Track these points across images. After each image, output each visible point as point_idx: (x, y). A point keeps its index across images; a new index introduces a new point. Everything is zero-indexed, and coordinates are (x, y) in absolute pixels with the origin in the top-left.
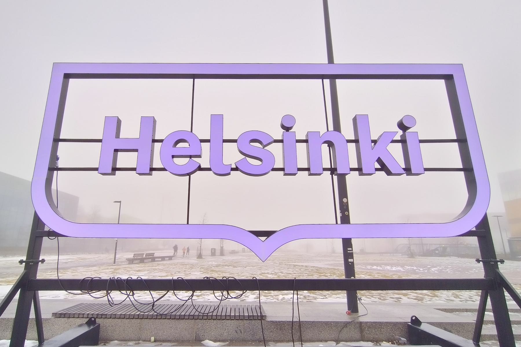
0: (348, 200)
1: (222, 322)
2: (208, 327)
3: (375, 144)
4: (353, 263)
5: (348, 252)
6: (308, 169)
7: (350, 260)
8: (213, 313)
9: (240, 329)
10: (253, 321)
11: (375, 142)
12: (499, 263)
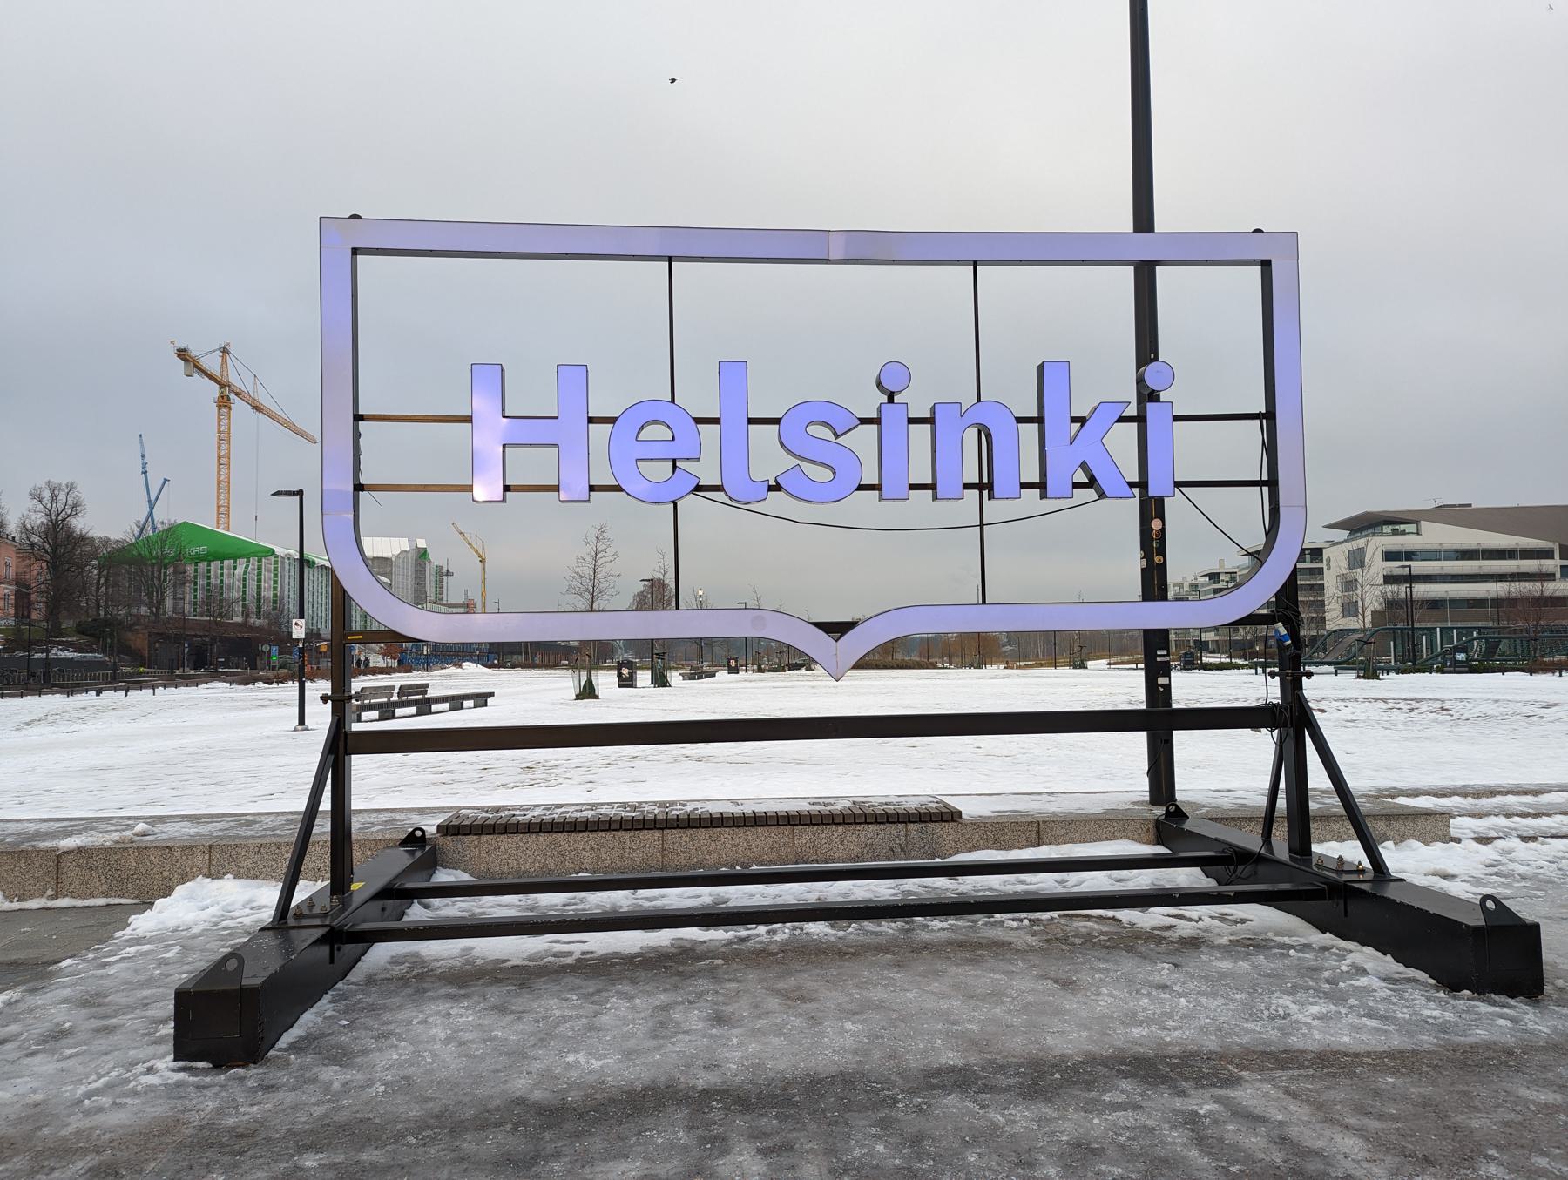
0: (1164, 524)
1: (858, 828)
2: (824, 841)
3: (1082, 426)
4: (1168, 687)
5: (1159, 659)
6: (932, 487)
7: (1161, 680)
8: (150, 501)
9: (900, 845)
10: (932, 825)
11: (1082, 421)
12: (1304, 678)
